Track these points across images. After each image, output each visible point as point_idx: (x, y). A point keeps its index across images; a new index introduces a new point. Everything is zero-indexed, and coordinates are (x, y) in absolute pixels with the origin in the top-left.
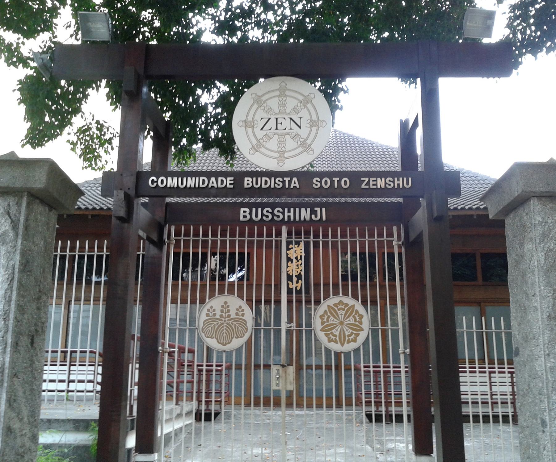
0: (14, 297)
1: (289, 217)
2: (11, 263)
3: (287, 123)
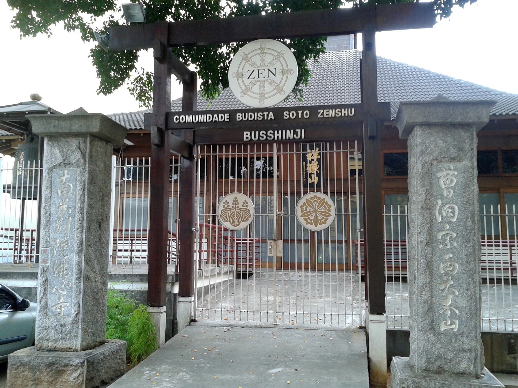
0: (86, 200)
1: (278, 137)
2: (83, 178)
3: (266, 73)
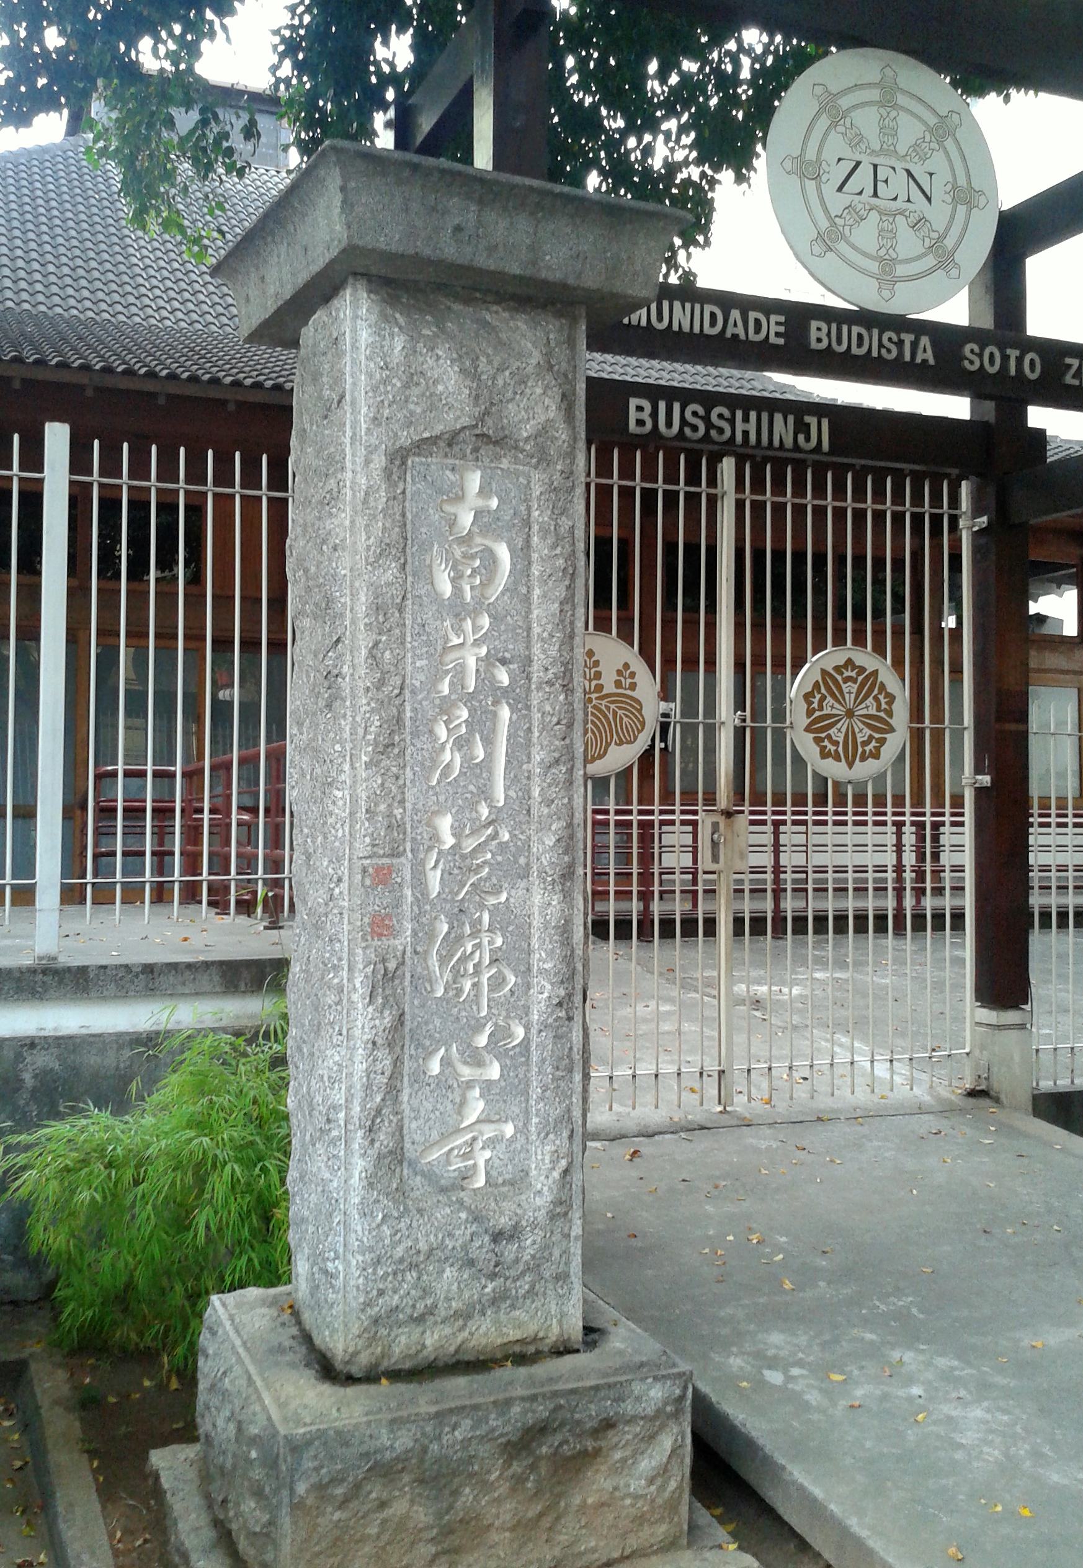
1: (746, 434)
2: (565, 523)
3: (899, 184)
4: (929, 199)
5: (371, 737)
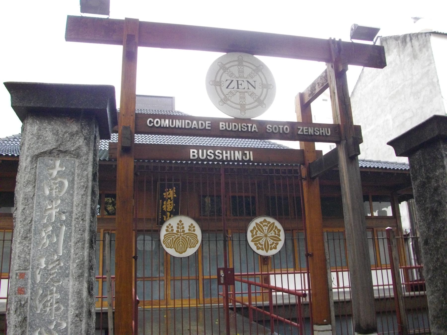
2: (86, 173)
3: (245, 85)
4: (255, 88)
5: (21, 235)
